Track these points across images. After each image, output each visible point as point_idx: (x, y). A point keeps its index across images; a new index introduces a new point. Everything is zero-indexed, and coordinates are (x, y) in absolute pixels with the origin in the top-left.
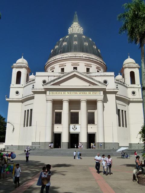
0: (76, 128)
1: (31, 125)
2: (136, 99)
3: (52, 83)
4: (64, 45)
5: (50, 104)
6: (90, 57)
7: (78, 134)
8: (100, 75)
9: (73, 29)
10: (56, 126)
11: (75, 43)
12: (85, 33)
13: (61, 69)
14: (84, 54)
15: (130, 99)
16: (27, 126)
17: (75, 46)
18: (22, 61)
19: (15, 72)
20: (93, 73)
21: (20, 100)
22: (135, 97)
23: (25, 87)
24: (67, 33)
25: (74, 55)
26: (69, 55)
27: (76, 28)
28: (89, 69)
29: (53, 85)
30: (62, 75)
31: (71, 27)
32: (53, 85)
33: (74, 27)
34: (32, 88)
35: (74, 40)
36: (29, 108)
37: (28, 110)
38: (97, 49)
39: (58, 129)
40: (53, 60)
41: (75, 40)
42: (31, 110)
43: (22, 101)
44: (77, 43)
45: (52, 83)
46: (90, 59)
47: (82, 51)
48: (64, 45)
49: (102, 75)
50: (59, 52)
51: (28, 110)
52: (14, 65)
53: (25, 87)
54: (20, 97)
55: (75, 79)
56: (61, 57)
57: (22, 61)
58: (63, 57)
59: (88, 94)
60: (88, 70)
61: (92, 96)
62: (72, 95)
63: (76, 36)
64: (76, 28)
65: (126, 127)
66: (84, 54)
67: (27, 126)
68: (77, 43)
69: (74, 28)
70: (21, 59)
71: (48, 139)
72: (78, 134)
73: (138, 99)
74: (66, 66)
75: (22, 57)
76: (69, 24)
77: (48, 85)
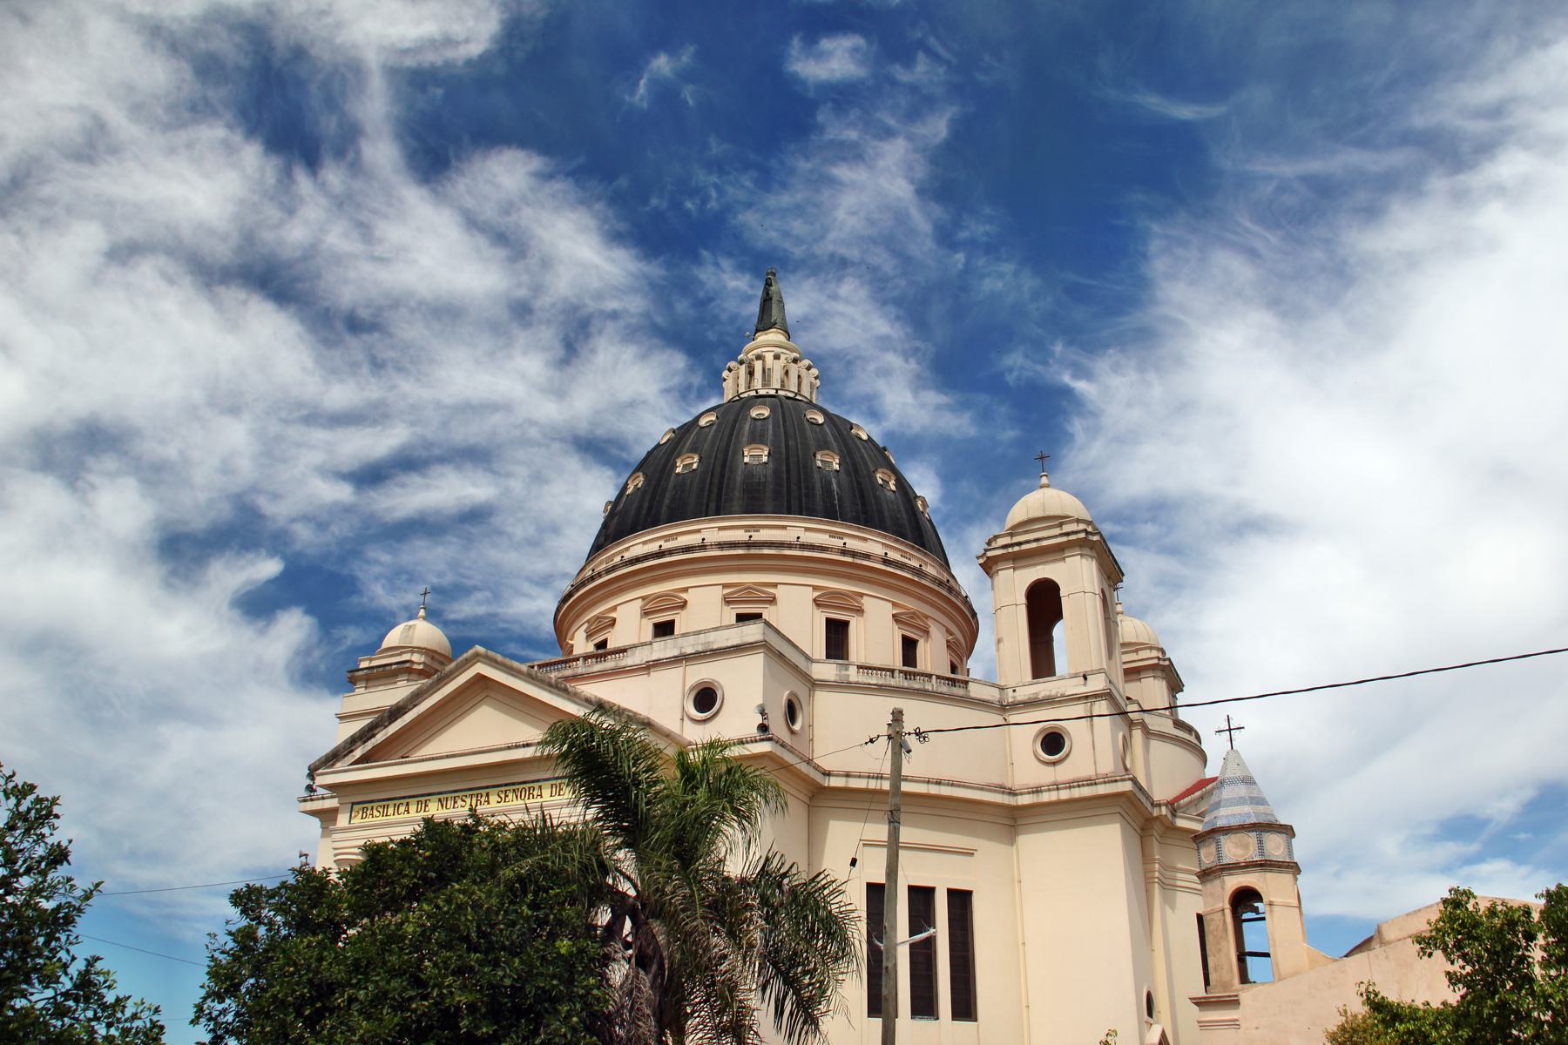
2: (1070, 785)
4: (678, 470)
6: (853, 544)
8: (676, 653)
9: (751, 373)
11: (756, 455)
13: (654, 624)
14: (807, 529)
15: (1012, 793)
20: (635, 646)
22: (1064, 772)
25: (741, 536)
26: (712, 531)
28: (846, 624)
29: (364, 759)
31: (741, 363)
32: (364, 759)
33: (759, 357)
34: (305, 794)
35: (745, 439)
40: (608, 571)
41: (757, 438)
44: (763, 453)
45: (358, 753)
46: (753, 551)
47: (794, 503)
48: (678, 470)
49: (689, 650)
56: (654, 547)
58: (667, 545)
63: (766, 412)
66: (807, 529)
68: (765, 459)
69: (758, 365)
73: (1091, 782)
74: (684, 605)
77: (339, 766)
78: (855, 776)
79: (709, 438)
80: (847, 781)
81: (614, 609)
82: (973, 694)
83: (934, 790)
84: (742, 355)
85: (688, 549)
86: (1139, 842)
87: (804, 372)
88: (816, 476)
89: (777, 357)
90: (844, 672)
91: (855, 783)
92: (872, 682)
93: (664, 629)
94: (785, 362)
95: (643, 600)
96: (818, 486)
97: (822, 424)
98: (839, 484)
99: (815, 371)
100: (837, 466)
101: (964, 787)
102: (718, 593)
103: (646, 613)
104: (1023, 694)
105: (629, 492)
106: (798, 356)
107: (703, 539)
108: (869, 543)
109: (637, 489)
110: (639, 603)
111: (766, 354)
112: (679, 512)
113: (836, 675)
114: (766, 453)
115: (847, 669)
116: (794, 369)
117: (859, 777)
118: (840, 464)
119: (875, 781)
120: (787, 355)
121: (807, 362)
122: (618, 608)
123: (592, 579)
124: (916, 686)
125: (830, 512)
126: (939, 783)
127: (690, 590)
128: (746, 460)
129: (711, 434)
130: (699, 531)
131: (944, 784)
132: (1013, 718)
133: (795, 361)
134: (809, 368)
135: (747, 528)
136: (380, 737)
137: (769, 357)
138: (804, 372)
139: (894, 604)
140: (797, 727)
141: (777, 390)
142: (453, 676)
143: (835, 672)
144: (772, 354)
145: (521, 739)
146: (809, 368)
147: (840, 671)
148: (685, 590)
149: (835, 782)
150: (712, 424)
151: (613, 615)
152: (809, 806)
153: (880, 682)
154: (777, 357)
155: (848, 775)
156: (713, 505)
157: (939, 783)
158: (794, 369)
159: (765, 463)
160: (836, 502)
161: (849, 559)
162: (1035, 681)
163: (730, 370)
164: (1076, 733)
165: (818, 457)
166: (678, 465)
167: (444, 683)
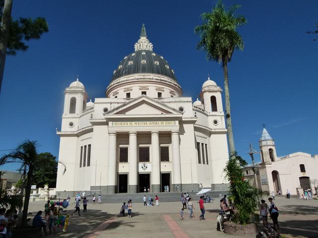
0: (147, 167)
1: (89, 165)
3: (115, 112)
5: (113, 138)
7: (169, 174)
9: (140, 45)
10: (121, 165)
11: (144, 62)
12: (154, 50)
16: (84, 166)
17: (143, 65)
18: (77, 85)
19: (68, 98)
21: (75, 133)
22: (217, 127)
23: (81, 116)
24: (133, 50)
26: (136, 76)
27: (144, 44)
28: (161, 93)
29: (117, 113)
30: (128, 101)
32: (117, 113)
35: (141, 58)
36: (87, 143)
37: (85, 146)
38: (170, 69)
39: (123, 168)
41: (144, 59)
42: (90, 146)
43: (78, 135)
45: (115, 112)
50: (124, 73)
51: (85, 146)
52: (67, 89)
53: (81, 116)
54: (74, 130)
55: (144, 105)
57: (77, 85)
58: (128, 79)
59: (160, 124)
60: (160, 94)
61: (165, 127)
62: (141, 126)
63: (145, 53)
64: (144, 44)
65: (208, 164)
67: (84, 166)
69: (141, 44)
70: (76, 82)
71: (112, 181)
72: (169, 174)
74: (132, 90)
75: (78, 80)
76: (136, 39)
77: (110, 114)
104: (210, 114)
125: (158, 73)
135: (143, 76)
136: (120, 109)
145: (156, 114)
150: (134, 56)
162: (84, 113)
164: (219, 122)
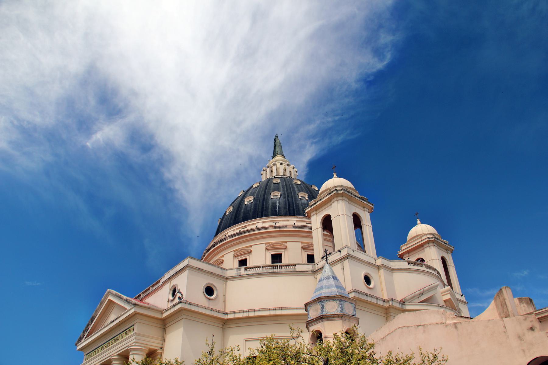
26: (260, 223)
31: (268, 167)
41: (277, 189)
56: (238, 231)
68: (279, 196)
74: (250, 252)
78: (238, 313)
79: (257, 192)
80: (234, 315)
81: (223, 256)
82: (297, 270)
83: (273, 313)
84: (268, 164)
85: (250, 230)
86: (167, 328)
87: (292, 170)
88: (270, 202)
89: (281, 164)
90: (239, 272)
91: (238, 316)
92: (250, 273)
93: (243, 263)
94: (284, 166)
95: (234, 251)
96: (270, 205)
97: (300, 184)
98: (279, 203)
99: (296, 169)
100: (307, 198)
101: (287, 309)
102: (264, 246)
103: (235, 256)
105: (227, 214)
106: (289, 163)
107: (257, 226)
108: (290, 221)
109: (230, 213)
110: (233, 253)
111: (277, 164)
112: (246, 218)
113: (236, 273)
114: (280, 194)
115: (240, 270)
116: (287, 168)
117: (239, 312)
118: (308, 197)
119: (246, 313)
120: (285, 164)
121: (292, 166)
122: (224, 256)
123: (214, 246)
124: (259, 272)
126: (275, 309)
127: (288, 243)
128: (272, 197)
129: (257, 191)
130: (255, 224)
131: (277, 310)
132: (393, 271)
133: (288, 165)
134: (293, 168)
137: (278, 165)
138: (292, 170)
139: (302, 243)
140: (371, 286)
141: (282, 176)
142: (104, 302)
143: (236, 272)
144: (279, 164)
146: (293, 168)
147: (237, 271)
148: (251, 246)
149: (230, 316)
150: (257, 187)
151: (223, 259)
152: (386, 317)
153: (254, 273)
154: (281, 164)
155: (234, 313)
156: (260, 214)
157: (275, 309)
158: (287, 168)
159: (280, 198)
160: (277, 209)
161: (278, 229)
163: (264, 170)
165: (299, 195)
166: (245, 201)
167: (102, 304)
